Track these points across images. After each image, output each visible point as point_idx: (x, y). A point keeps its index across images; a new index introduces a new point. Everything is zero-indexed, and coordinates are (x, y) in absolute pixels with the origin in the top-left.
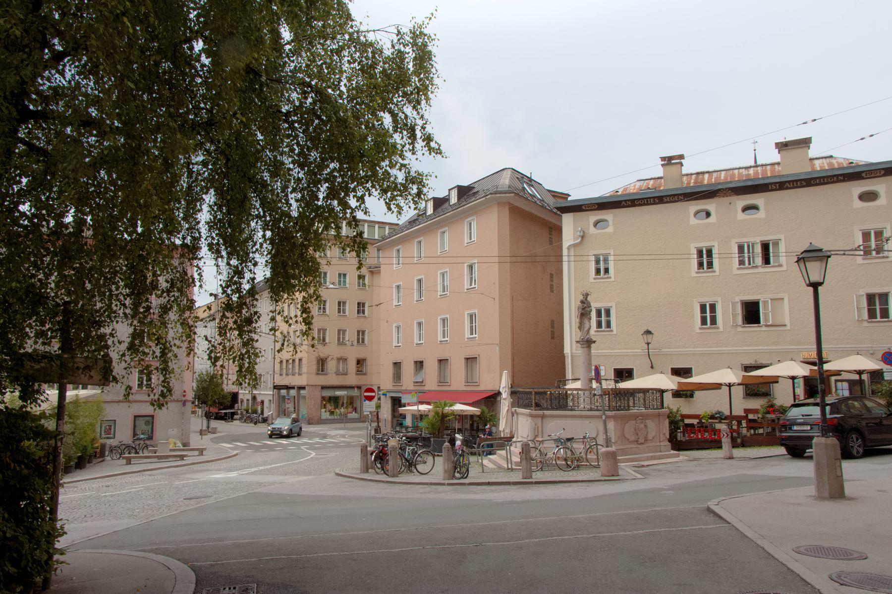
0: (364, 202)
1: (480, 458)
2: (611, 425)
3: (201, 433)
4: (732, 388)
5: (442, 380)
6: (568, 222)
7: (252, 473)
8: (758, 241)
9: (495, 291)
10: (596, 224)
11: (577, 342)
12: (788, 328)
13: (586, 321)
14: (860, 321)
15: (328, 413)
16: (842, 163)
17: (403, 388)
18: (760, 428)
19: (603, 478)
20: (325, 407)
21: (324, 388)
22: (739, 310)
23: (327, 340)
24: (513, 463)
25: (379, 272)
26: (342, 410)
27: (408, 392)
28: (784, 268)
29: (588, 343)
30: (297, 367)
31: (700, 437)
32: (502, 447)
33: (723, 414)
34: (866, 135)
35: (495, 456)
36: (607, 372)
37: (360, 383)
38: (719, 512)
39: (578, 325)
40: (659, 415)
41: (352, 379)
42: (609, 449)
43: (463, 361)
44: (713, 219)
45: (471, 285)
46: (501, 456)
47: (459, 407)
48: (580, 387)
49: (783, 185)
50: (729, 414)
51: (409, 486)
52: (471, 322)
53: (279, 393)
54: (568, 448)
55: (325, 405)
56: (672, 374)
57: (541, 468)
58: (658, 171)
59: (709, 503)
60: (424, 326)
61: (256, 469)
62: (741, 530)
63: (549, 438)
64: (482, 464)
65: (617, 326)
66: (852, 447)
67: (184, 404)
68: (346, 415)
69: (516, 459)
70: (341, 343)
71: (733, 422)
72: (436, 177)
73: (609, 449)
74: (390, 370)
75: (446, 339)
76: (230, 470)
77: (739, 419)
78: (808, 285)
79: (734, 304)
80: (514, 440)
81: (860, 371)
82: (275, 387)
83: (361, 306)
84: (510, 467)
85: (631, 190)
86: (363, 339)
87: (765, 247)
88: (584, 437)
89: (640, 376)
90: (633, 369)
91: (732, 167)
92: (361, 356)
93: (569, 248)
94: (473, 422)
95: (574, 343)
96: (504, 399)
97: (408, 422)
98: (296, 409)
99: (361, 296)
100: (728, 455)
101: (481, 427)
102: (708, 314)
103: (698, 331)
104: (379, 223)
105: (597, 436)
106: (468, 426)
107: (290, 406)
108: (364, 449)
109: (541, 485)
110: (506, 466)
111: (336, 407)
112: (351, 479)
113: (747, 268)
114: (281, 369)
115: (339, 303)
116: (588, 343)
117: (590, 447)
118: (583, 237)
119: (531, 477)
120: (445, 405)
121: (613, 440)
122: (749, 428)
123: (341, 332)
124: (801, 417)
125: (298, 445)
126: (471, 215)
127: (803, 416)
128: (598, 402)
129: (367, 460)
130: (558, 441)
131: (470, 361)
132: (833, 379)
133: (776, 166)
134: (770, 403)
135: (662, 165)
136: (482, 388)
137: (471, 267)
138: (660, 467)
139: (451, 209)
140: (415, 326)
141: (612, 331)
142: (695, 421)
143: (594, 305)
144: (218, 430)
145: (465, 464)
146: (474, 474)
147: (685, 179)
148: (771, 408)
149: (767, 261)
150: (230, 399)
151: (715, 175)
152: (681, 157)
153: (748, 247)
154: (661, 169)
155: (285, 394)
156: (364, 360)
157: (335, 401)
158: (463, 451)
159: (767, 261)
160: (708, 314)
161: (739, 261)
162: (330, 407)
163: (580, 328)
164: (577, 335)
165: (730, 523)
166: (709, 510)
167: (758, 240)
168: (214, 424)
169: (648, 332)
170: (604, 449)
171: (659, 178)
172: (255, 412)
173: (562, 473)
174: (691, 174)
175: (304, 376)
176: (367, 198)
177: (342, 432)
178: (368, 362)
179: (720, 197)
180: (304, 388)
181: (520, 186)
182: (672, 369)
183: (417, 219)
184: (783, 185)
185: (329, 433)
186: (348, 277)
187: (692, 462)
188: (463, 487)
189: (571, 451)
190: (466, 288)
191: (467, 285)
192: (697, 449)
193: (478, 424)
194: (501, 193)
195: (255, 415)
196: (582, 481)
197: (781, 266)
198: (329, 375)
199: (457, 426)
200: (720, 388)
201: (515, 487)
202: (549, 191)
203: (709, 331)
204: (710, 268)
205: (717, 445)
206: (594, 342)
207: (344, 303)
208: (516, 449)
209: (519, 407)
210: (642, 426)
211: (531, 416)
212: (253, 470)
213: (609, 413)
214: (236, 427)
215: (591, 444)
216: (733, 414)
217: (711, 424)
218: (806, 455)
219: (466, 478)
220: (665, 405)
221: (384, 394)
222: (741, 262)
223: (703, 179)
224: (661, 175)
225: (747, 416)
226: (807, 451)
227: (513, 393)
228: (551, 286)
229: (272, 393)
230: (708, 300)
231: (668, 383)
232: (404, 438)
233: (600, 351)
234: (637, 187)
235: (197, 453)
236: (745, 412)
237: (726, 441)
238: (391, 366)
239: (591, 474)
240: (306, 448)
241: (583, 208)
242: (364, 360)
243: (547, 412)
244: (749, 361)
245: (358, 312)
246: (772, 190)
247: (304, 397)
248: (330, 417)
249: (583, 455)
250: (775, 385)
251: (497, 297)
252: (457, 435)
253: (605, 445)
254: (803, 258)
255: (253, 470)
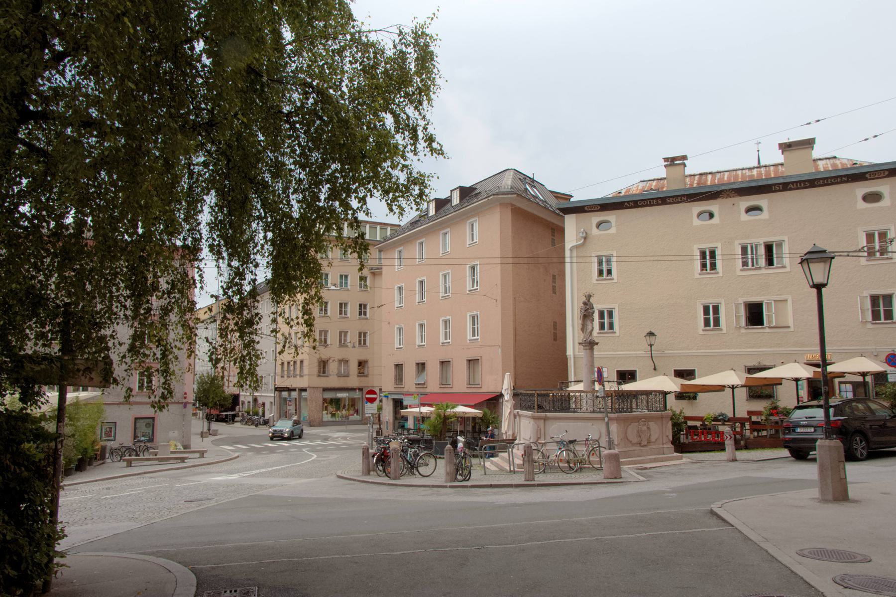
0: (365, 203)
1: (482, 460)
2: (614, 427)
3: (202, 435)
4: (735, 390)
5: (444, 382)
6: (571, 224)
7: (253, 476)
8: (762, 242)
9: (497, 293)
10: (598, 225)
11: (580, 344)
12: (792, 329)
13: (589, 323)
14: (864, 323)
15: (330, 415)
16: (846, 164)
17: (405, 390)
18: (763, 430)
19: (606, 481)
20: (326, 409)
21: (325, 390)
22: (742, 311)
23: (329, 342)
24: (516, 466)
25: (381, 274)
26: (344, 412)
27: (410, 394)
28: (788, 269)
29: (590, 345)
30: (298, 369)
31: (703, 439)
32: (504, 449)
33: (726, 416)
34: (870, 136)
35: (497, 458)
36: (610, 374)
37: (361, 385)
38: (722, 515)
39: (580, 326)
40: (662, 417)
41: (354, 381)
42: (612, 451)
43: (465, 362)
44: (716, 220)
45: (473, 286)
46: (503, 458)
47: (461, 409)
48: (582, 389)
49: (786, 186)
50: (732, 416)
51: (411, 488)
52: (474, 324)
53: (280, 395)
54: (571, 451)
55: (326, 407)
56: (675, 376)
57: (544, 471)
58: (661, 172)
59: (712, 506)
60: (426, 328)
61: (257, 472)
62: (744, 532)
63: (551, 440)
64: (484, 467)
65: (620, 327)
66: (856, 449)
67: (185, 407)
68: (347, 417)
69: (518, 461)
70: (342, 344)
71: (737, 424)
72: (438, 178)
73: (612, 451)
74: (391, 372)
75: (448, 341)
76: (231, 472)
77: (742, 421)
78: (812, 287)
79: (737, 306)
80: (516, 442)
81: (864, 372)
82: (276, 389)
83: (362, 308)
84: (512, 469)
85: (634, 191)
86: (365, 341)
87: (769, 248)
88: (587, 440)
89: (643, 378)
90: (635, 371)
91: (735, 167)
92: (363, 358)
93: (571, 250)
94: (475, 424)
95: (577, 344)
96: (507, 401)
97: (410, 424)
98: (297, 411)
99: (362, 298)
100: (731, 458)
101: (483, 429)
102: (711, 316)
103: (701, 333)
104: (381, 224)
105: (600, 438)
106: (470, 428)
107: (291, 408)
108: (365, 452)
109: (543, 488)
110: (508, 468)
111: (338, 409)
112: (352, 482)
113: (750, 269)
114: (282, 370)
115: (341, 305)
116: (590, 345)
117: (593, 449)
118: (585, 238)
119: (533, 480)
120: (447, 407)
121: (616, 443)
122: (752, 430)
123: (343, 334)
124: (805, 419)
125: (300, 448)
126: (473, 216)
127: (806, 418)
128: (601, 404)
129: (369, 462)
130: (561, 443)
131: (472, 363)
132: (837, 380)
133: (780, 167)
134: (773, 405)
135: (665, 166)
136: (484, 390)
137: (473, 268)
138: (663, 469)
139: (453, 210)
140: (417, 327)
141: (615, 333)
142: (698, 424)
143: (597, 307)
144: (219, 432)
145: (467, 467)
146: (477, 476)
147: (688, 179)
148: (774, 410)
149: (770, 262)
150: (231, 401)
151: (718, 176)
152: (684, 158)
153: (752, 248)
154: (664, 169)
155: (287, 396)
156: (366, 362)
157: (336, 403)
158: (465, 453)
159: (770, 262)
160: (711, 316)
161: (743, 262)
162: (331, 409)
163: (583, 329)
164: (580, 337)
165: (733, 526)
166: (713, 513)
167: (761, 241)
168: (215, 426)
169: (651, 334)
170: (607, 452)
171: (661, 179)
172: (256, 414)
173: (565, 476)
174: (695, 175)
175: (306, 378)
176: (368, 199)
177: (343, 434)
178: (370, 364)
179: (723, 198)
180: (305, 390)
181: (522, 187)
182: (675, 371)
183: (419, 221)
184: (786, 186)
185: (330, 435)
186: (349, 278)
187: (695, 464)
188: (466, 489)
189: (574, 453)
190: (468, 289)
191: (469, 287)
192: (701, 451)
193: (480, 426)
194: (503, 193)
195: (256, 417)
196: (585, 484)
197: (784, 267)
198: (331, 377)
199: (459, 428)
200: (724, 390)
201: (517, 490)
202: (552, 192)
203: (712, 333)
204: (713, 269)
205: (720, 447)
206: (597, 344)
207: (346, 304)
208: (518, 451)
209: (521, 409)
210: (645, 428)
211: (534, 418)
212: (254, 472)
213: (611, 415)
214: (237, 429)
215: (594, 446)
216: (736, 416)
217: (714, 426)
218: (810, 457)
219: (468, 480)
220: (668, 407)
221: (385, 396)
222: (745, 264)
223: (706, 180)
224: (664, 175)
225: (750, 418)
226: (811, 453)
227: (515, 395)
228: (554, 288)
229: (273, 395)
230: (711, 301)
231: (671, 384)
232: (406, 440)
233: (602, 353)
234: (639, 188)
235: (198, 455)
236: (748, 415)
237: (729, 443)
238: (393, 368)
239: (594, 476)
240: (308, 451)
241: (586, 209)
242: (366, 362)
243: (549, 415)
244: (753, 363)
245: (360, 314)
246: (776, 191)
247: (306, 399)
248: (331, 419)
249: (586, 457)
250: (778, 387)
251: (499, 299)
252: (459, 438)
253: (608, 448)
254: (807, 259)
255: (254, 472)
